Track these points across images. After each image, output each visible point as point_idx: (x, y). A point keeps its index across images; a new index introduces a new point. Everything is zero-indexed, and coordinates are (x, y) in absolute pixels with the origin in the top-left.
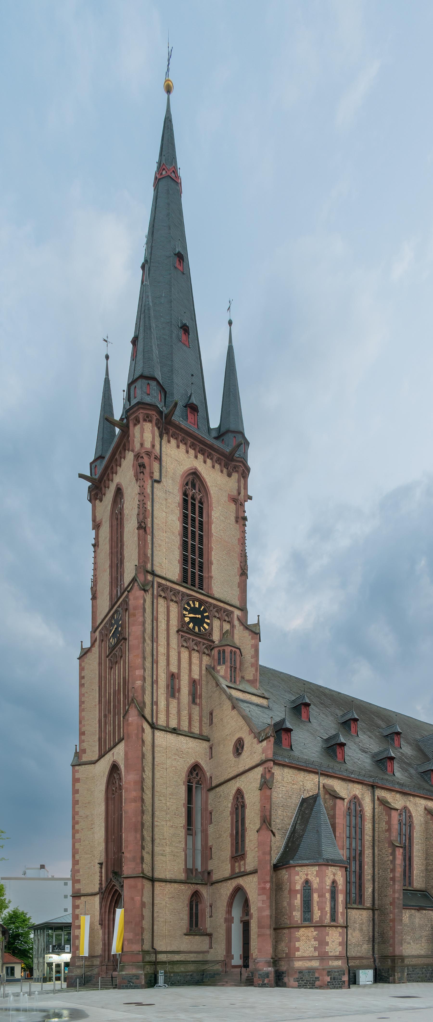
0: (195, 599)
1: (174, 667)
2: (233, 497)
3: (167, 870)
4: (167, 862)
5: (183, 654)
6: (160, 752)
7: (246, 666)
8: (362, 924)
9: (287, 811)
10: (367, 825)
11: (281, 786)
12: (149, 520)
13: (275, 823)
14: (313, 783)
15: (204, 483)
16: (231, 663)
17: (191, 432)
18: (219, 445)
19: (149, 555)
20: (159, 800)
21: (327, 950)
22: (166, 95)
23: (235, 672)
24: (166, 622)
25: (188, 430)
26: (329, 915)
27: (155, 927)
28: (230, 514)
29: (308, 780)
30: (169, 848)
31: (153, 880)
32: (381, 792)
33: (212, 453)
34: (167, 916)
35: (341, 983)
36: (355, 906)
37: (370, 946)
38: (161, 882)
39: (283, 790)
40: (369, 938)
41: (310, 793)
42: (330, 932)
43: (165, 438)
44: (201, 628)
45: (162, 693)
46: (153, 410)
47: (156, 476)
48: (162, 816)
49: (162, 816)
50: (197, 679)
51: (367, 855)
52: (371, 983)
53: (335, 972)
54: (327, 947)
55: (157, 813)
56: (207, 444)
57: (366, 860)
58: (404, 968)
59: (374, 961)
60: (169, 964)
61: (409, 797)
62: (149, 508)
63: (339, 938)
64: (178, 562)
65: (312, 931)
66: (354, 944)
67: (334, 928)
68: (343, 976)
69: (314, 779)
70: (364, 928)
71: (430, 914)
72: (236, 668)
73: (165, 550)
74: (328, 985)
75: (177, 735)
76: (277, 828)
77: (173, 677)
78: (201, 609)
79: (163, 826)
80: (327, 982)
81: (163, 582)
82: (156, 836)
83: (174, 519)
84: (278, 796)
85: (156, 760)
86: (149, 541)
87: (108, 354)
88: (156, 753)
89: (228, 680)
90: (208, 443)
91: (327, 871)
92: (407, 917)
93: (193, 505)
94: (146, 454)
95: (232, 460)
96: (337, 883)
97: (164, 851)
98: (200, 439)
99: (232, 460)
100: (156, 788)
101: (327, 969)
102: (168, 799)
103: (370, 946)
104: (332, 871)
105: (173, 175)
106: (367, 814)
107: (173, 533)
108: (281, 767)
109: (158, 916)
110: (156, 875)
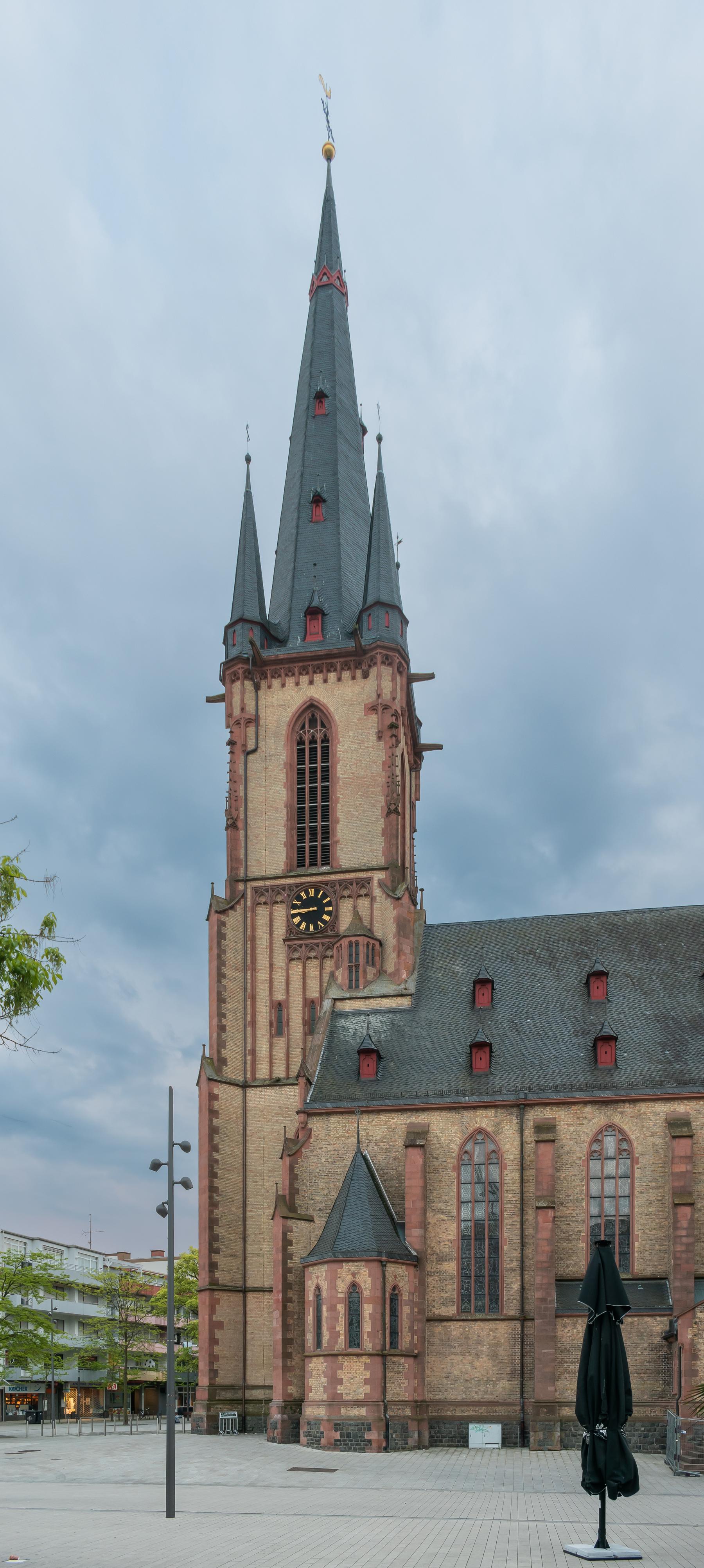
0: (306, 888)
1: (281, 993)
2: (371, 706)
3: (265, 1275)
4: (265, 1264)
6: (255, 1117)
8: (497, 1345)
9: (335, 1180)
10: (509, 1175)
11: (325, 1145)
13: (313, 1202)
16: (350, 961)
17: (295, 655)
19: (242, 857)
20: (254, 1182)
21: (339, 1392)
22: (326, 163)
23: (357, 971)
25: (289, 656)
26: (342, 1337)
27: (249, 1354)
28: (369, 733)
29: (375, 1125)
30: (268, 1245)
31: (244, 1291)
32: (541, 1112)
34: (266, 1337)
35: (362, 1443)
36: (479, 1316)
37: (516, 1383)
38: (257, 1293)
39: (328, 1150)
40: (514, 1370)
41: (381, 1144)
42: (346, 1364)
44: (319, 922)
45: (263, 1035)
46: (239, 663)
47: (251, 746)
48: (257, 1202)
49: (257, 1202)
51: (509, 1227)
52: (496, 1446)
53: (350, 1425)
54: (339, 1387)
55: (250, 1200)
56: (321, 655)
57: (505, 1235)
58: (552, 1423)
59: (523, 1409)
60: (265, 1403)
61: (621, 1105)
62: (241, 794)
63: (364, 1372)
64: (284, 845)
65: (322, 1363)
66: (476, 1379)
67: (355, 1358)
68: (366, 1432)
69: (390, 1121)
70: (501, 1352)
71: (646, 1322)
72: (359, 965)
74: (335, 1444)
76: (318, 1208)
77: (279, 1008)
78: (319, 897)
79: (259, 1216)
80: (333, 1441)
81: (261, 883)
82: (250, 1231)
85: (249, 1128)
87: (250, 454)
88: (249, 1119)
89: (344, 988)
90: (322, 653)
91: (339, 1270)
92: (578, 1332)
93: (313, 751)
95: (365, 652)
96: (360, 1287)
97: (261, 1250)
98: (311, 656)
99: (365, 652)
100: (250, 1167)
101: (333, 1420)
102: (266, 1178)
103: (516, 1383)
104: (350, 1270)
105: (338, 283)
106: (509, 1157)
108: (325, 1117)
109: (253, 1338)
110: (250, 1283)
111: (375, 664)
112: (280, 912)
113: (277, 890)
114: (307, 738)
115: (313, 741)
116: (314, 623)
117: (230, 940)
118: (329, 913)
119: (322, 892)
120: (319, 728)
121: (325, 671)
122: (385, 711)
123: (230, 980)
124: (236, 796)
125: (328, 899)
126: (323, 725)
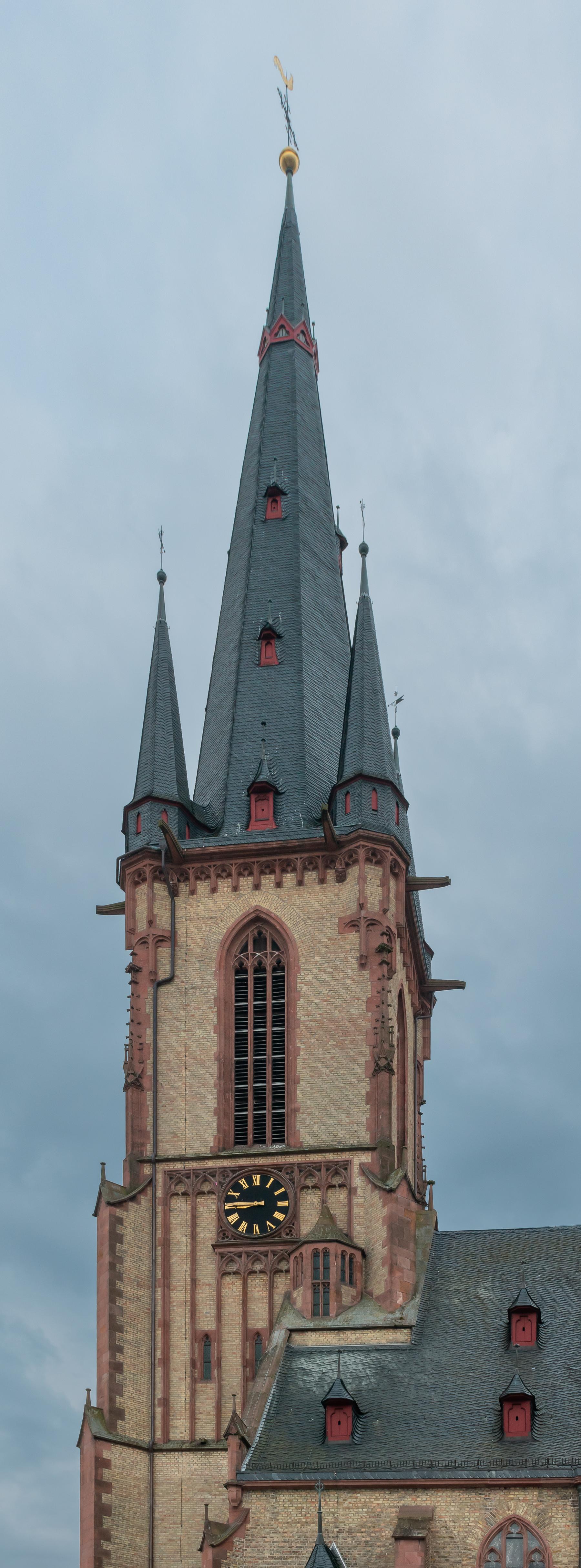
1: (208, 1321)
5: (229, 1288)
7: (375, 1267)
11: (269, 1533)
12: (150, 1062)
14: (366, 1512)
15: (278, 927)
16: (315, 1276)
18: (300, 837)
23: (326, 1292)
24: (189, 1240)
29: (349, 1508)
33: (290, 859)
39: (275, 1540)
43: (183, 889)
44: (268, 1222)
45: (180, 1379)
47: (164, 972)
50: (262, 1329)
72: (329, 1284)
73: (183, 1104)
75: (207, 1453)
78: (268, 1186)
83: (205, 1033)
84: (258, 1557)
86: (150, 1102)
88: (159, 1496)
90: (274, 846)
93: (260, 983)
94: (142, 943)
95: (340, 845)
107: (203, 1062)
108: (270, 1494)
111: (356, 861)
112: (208, 1208)
113: (204, 1176)
114: (250, 964)
115: (260, 968)
116: (263, 804)
117: (129, 1244)
118: (283, 1210)
119: (272, 1180)
120: (269, 950)
121: (278, 871)
122: (371, 927)
123: (129, 1299)
124: (141, 1044)
125: (283, 1190)
126: (275, 947)
